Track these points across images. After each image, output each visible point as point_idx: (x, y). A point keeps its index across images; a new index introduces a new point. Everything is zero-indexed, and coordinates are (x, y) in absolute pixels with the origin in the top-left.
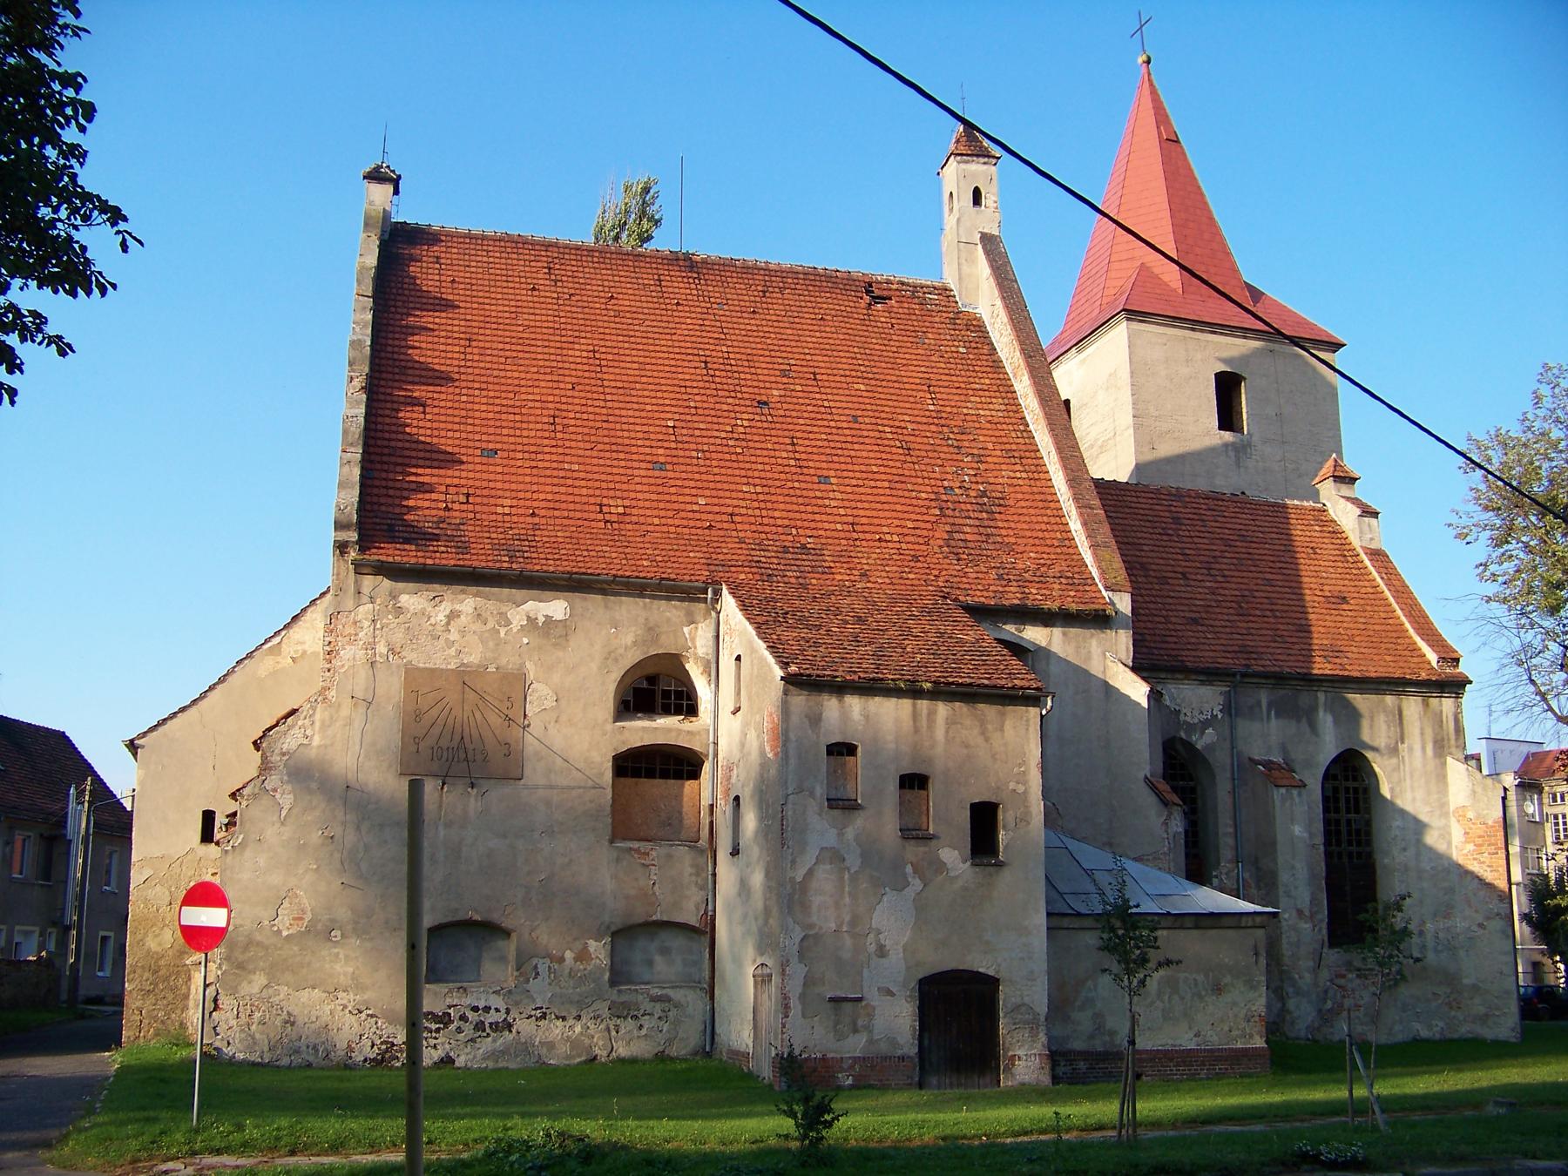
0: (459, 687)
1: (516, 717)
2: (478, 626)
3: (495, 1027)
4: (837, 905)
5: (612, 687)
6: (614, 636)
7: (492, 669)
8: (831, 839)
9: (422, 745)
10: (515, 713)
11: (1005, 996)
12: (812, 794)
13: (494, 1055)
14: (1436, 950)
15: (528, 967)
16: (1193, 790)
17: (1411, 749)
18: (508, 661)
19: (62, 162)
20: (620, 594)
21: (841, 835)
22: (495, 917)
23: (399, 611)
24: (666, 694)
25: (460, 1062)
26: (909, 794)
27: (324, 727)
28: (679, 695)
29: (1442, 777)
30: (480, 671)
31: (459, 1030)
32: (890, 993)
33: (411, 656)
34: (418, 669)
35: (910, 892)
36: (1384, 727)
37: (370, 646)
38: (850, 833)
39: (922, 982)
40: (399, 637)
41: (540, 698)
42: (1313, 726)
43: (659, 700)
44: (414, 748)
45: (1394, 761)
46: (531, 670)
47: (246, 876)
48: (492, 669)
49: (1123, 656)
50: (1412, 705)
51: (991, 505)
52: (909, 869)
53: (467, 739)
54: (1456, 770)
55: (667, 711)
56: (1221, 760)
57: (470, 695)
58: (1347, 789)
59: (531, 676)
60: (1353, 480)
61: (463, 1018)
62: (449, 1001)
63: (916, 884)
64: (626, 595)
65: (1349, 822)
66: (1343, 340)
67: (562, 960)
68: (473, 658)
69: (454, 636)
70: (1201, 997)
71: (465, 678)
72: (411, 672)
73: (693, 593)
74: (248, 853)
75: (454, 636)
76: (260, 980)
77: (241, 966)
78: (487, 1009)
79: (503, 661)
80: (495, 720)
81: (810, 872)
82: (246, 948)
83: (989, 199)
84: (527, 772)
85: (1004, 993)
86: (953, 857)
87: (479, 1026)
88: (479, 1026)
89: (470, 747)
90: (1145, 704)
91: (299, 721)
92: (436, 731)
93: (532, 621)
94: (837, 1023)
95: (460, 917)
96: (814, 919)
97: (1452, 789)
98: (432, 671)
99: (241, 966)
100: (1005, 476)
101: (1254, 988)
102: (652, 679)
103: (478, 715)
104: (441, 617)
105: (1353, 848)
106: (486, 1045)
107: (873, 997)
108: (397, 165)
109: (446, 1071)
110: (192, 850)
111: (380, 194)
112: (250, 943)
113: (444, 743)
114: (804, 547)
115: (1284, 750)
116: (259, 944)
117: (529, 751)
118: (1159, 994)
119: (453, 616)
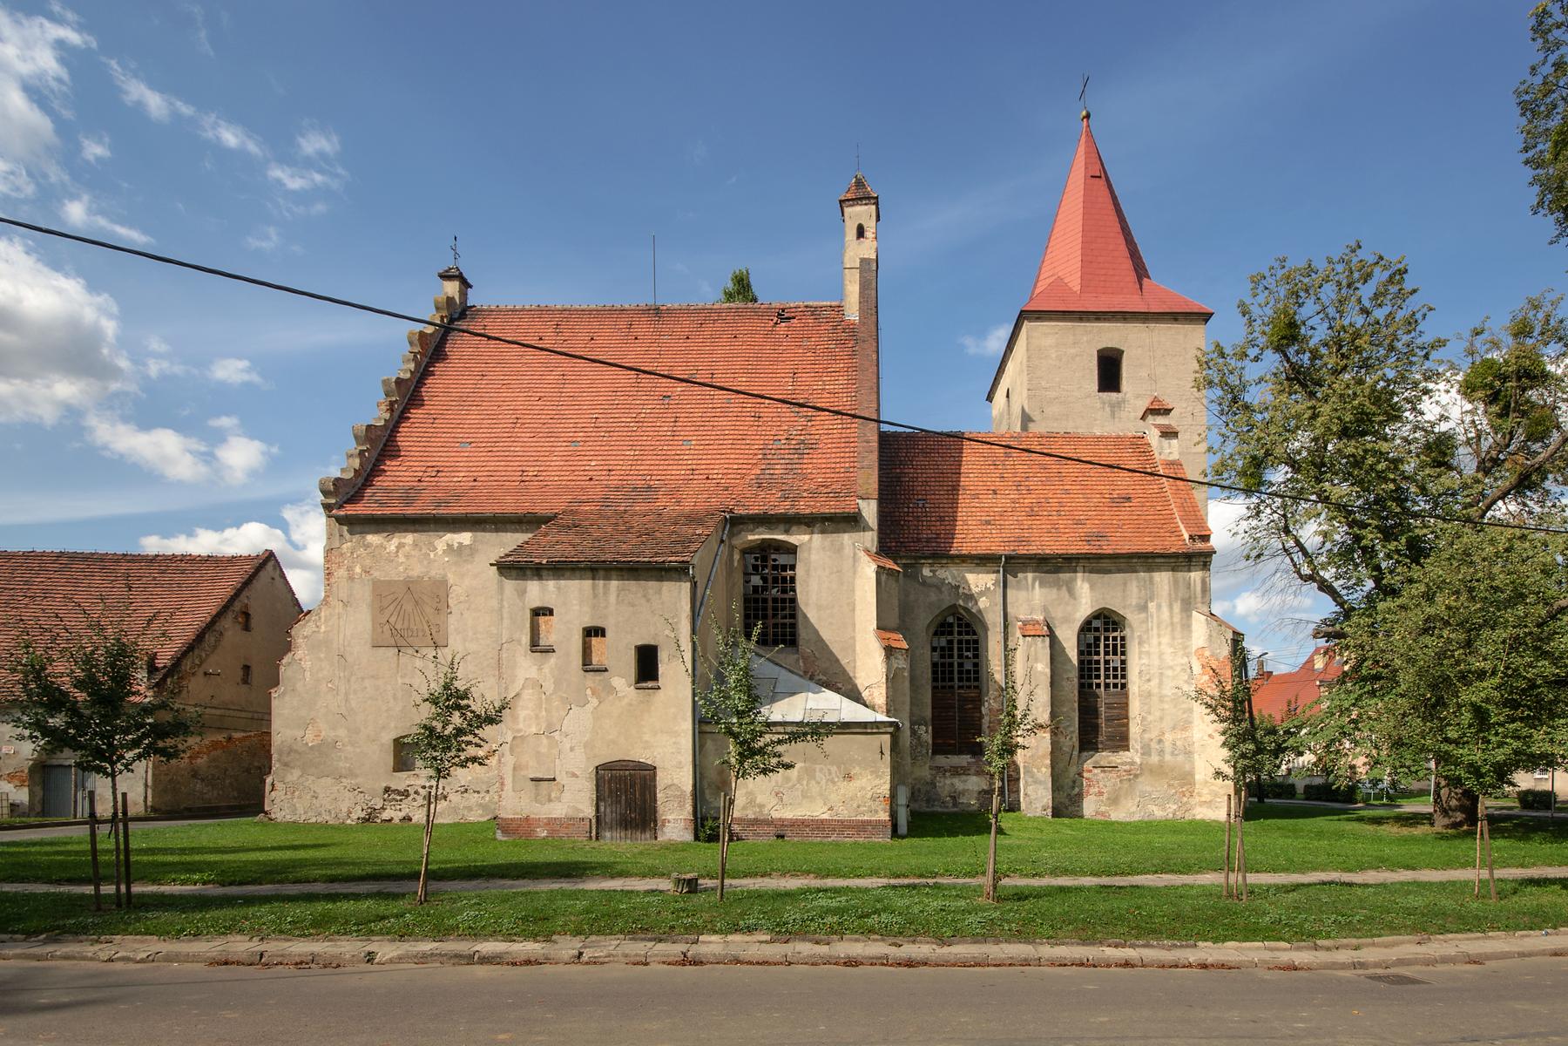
8: (533, 673)
11: (662, 780)
12: (519, 641)
14: (1172, 754)
16: (976, 642)
17: (1159, 607)
18: (435, 572)
20: (1110, 572)
21: (540, 669)
23: (367, 546)
32: (574, 775)
33: (376, 574)
35: (589, 707)
36: (1135, 590)
37: (349, 569)
38: (546, 669)
42: (1071, 592)
45: (1143, 615)
46: (451, 579)
49: (869, 545)
50: (1163, 579)
52: (589, 692)
54: (1199, 621)
56: (993, 619)
58: (1107, 639)
59: (451, 582)
60: (1167, 412)
63: (594, 702)
64: (1119, 571)
65: (1107, 662)
66: (1210, 310)
68: (417, 571)
69: (402, 559)
70: (834, 783)
74: (287, 698)
75: (402, 559)
76: (296, 773)
77: (286, 765)
79: (433, 573)
83: (869, 234)
85: (660, 775)
86: (622, 680)
93: (450, 546)
94: (537, 795)
96: (521, 726)
97: (1195, 635)
99: (286, 765)
101: (880, 777)
105: (1111, 681)
107: (562, 778)
109: (406, 824)
112: (291, 751)
114: (650, 487)
115: (1045, 609)
118: (799, 780)
119: (400, 546)
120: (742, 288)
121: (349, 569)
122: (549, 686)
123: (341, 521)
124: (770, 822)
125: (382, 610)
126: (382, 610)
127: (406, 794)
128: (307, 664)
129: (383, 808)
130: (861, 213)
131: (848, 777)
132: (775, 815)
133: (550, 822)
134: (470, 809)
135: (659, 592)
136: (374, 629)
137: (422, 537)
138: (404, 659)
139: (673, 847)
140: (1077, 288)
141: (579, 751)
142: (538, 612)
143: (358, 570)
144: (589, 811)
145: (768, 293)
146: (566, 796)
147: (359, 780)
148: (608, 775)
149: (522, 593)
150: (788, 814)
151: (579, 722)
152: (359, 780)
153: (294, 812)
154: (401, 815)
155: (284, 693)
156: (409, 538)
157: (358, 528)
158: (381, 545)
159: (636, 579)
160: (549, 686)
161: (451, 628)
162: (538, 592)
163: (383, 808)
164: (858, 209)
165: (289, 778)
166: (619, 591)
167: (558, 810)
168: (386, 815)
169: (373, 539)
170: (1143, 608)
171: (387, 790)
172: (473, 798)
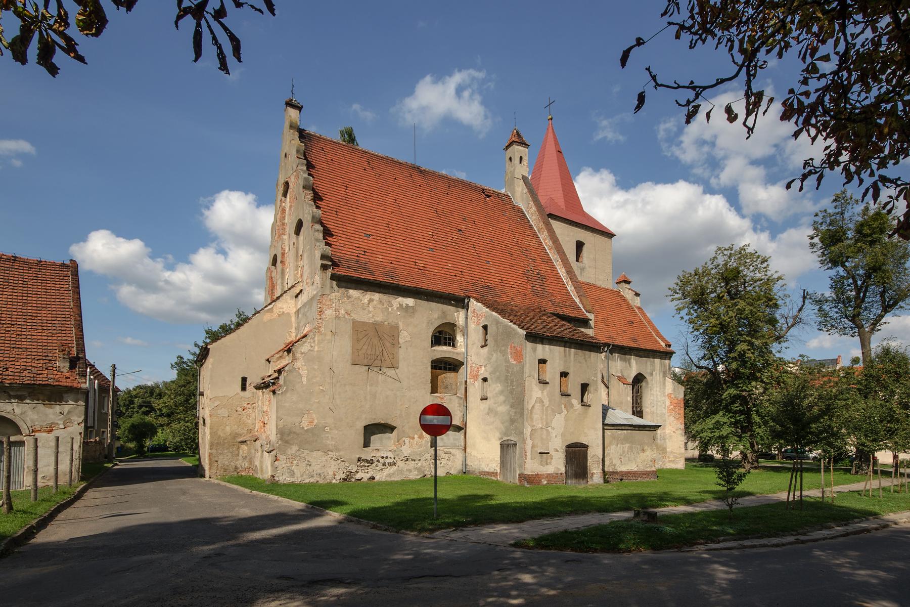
2: (380, 306)
3: (390, 464)
4: (542, 419)
5: (430, 334)
6: (431, 314)
11: (590, 453)
13: (389, 475)
15: (401, 441)
22: (390, 422)
23: (349, 297)
24: (445, 338)
25: (377, 478)
26: (563, 379)
27: (319, 343)
28: (449, 339)
29: (664, 383)
30: (381, 324)
31: (377, 466)
32: (557, 451)
33: (355, 316)
39: (568, 446)
40: (349, 307)
43: (443, 341)
47: (287, 404)
48: (386, 323)
50: (657, 361)
51: (541, 278)
55: (445, 344)
59: (401, 327)
61: (378, 461)
62: (372, 455)
63: (565, 412)
67: (413, 438)
68: (379, 318)
69: (371, 309)
73: (460, 302)
74: (288, 395)
75: (371, 309)
76: (295, 448)
77: (287, 442)
78: (387, 457)
79: (390, 321)
81: (533, 407)
82: (289, 435)
87: (384, 464)
88: (384, 464)
91: (308, 339)
95: (376, 422)
98: (363, 323)
99: (287, 442)
100: (544, 268)
102: (440, 332)
104: (366, 301)
106: (387, 471)
107: (552, 452)
108: (297, 99)
110: (238, 394)
111: (293, 113)
112: (290, 432)
116: (294, 433)
119: (371, 301)
120: (349, 136)
121: (337, 310)
122: (546, 402)
123: (333, 277)
124: (617, 473)
125: (358, 340)
126: (358, 340)
127: (371, 462)
128: (304, 372)
129: (357, 472)
130: (517, 150)
131: (643, 451)
132: (619, 469)
133: (549, 476)
134: (410, 471)
135: (590, 357)
136: (353, 353)
137: (385, 297)
138: (372, 374)
139: (596, 487)
140: (563, 207)
141: (559, 437)
142: (542, 362)
143: (342, 312)
144: (563, 469)
145: (363, 143)
146: (553, 462)
147: (342, 453)
148: (570, 450)
149: (535, 350)
150: (624, 469)
151: (558, 422)
152: (342, 453)
153: (292, 474)
154: (369, 476)
155: (286, 391)
156: (377, 296)
157: (344, 284)
158: (359, 298)
159: (581, 349)
160: (546, 402)
161: (401, 357)
162: (543, 350)
163: (357, 472)
164: (520, 148)
165: (289, 452)
166: (576, 354)
167: (550, 469)
168: (358, 476)
169: (353, 293)
170: (652, 374)
171: (359, 460)
172: (411, 464)
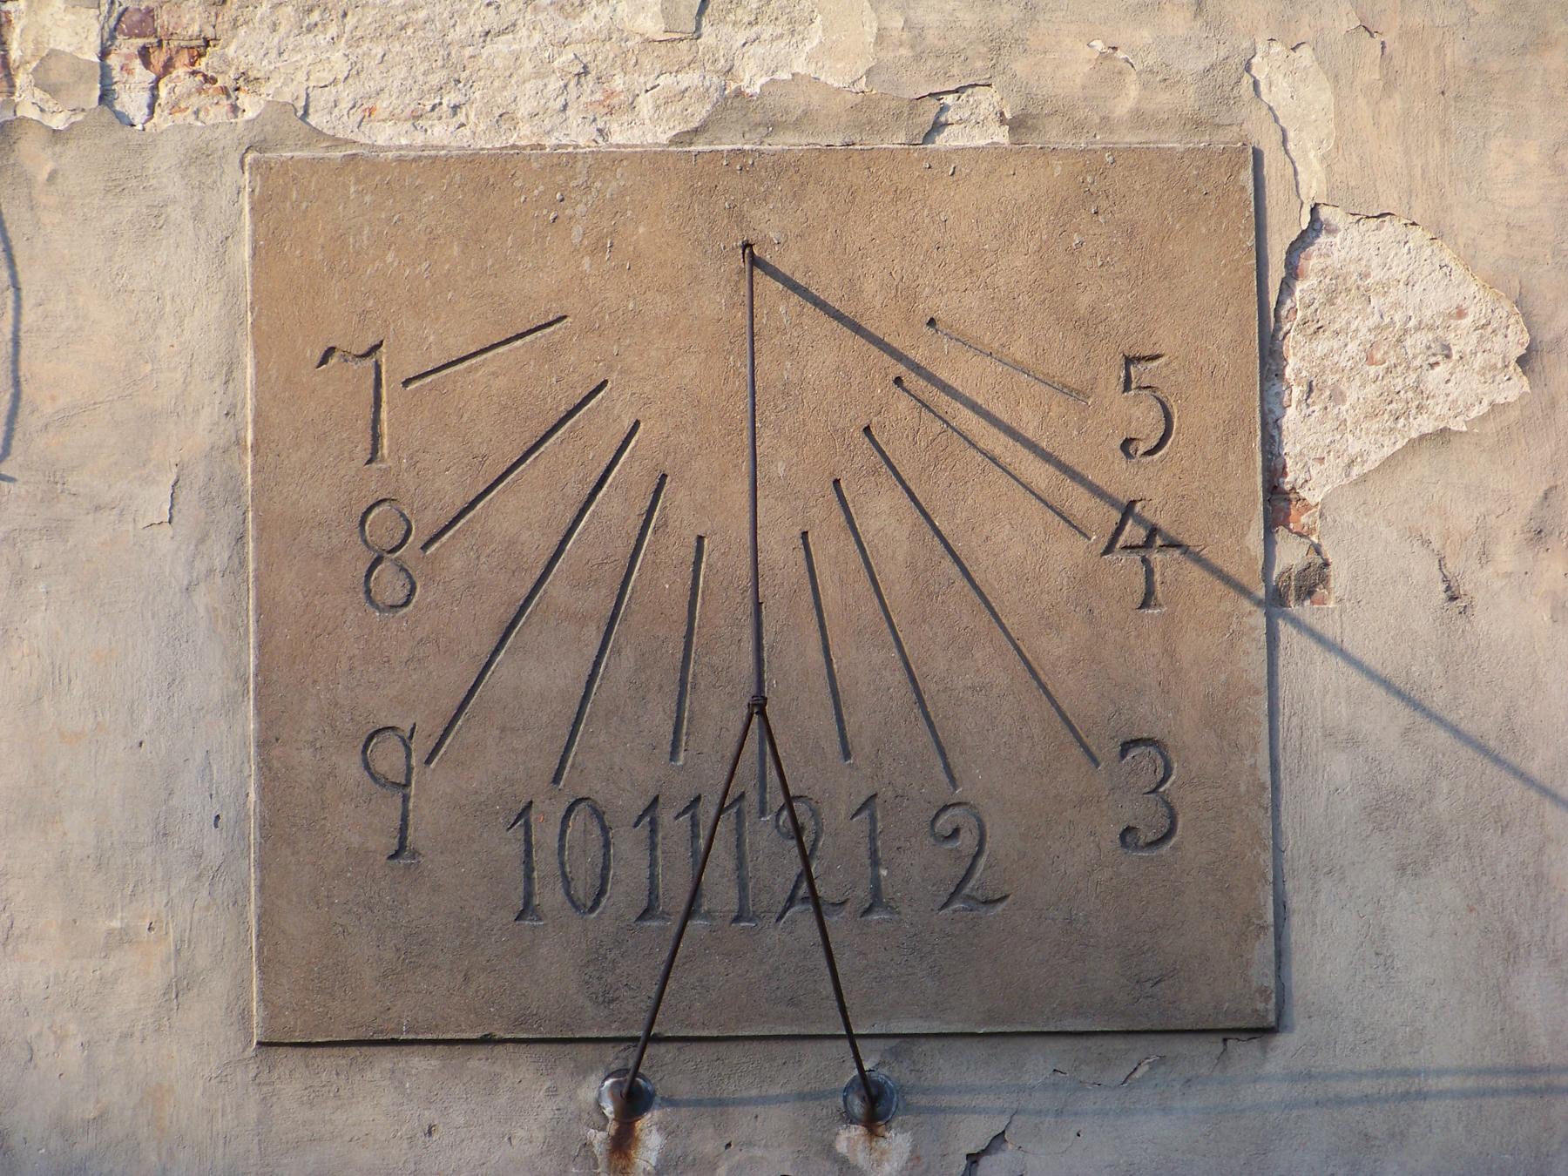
0: (716, 300)
1: (1206, 528)
7: (975, 128)
9: (435, 791)
10: (1200, 488)
19: (1317, 107)
34: (359, 163)
41: (1390, 363)
44: (363, 826)
46: (1306, 116)
48: (975, 128)
53: (801, 719)
57: (813, 359)
59: (1306, 170)
71: (753, 213)
72: (301, 189)
79: (1066, 62)
80: (1025, 545)
84: (1325, 956)
89: (833, 789)
90: (1280, 622)
92: (543, 672)
98: (485, 175)
103: (883, 515)
113: (621, 765)
117: (1326, 791)
